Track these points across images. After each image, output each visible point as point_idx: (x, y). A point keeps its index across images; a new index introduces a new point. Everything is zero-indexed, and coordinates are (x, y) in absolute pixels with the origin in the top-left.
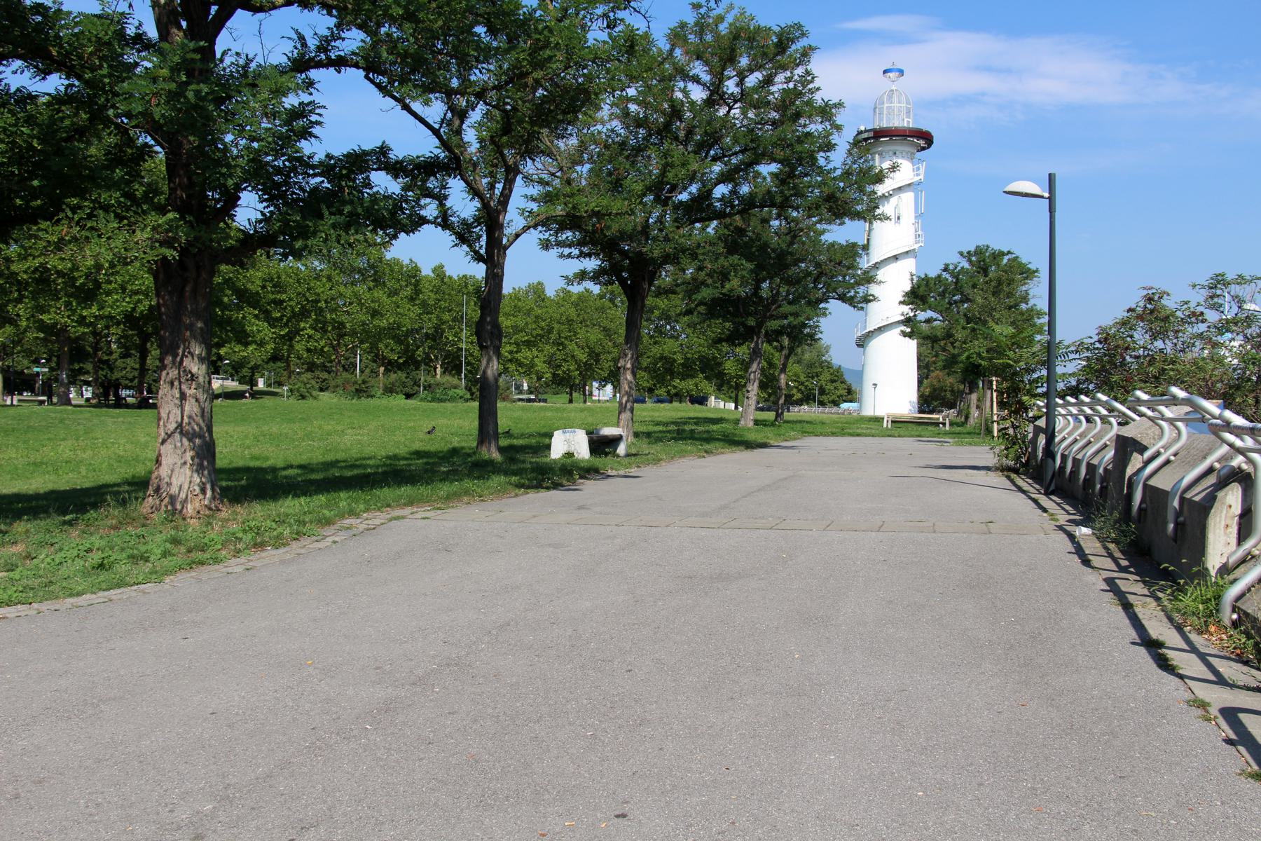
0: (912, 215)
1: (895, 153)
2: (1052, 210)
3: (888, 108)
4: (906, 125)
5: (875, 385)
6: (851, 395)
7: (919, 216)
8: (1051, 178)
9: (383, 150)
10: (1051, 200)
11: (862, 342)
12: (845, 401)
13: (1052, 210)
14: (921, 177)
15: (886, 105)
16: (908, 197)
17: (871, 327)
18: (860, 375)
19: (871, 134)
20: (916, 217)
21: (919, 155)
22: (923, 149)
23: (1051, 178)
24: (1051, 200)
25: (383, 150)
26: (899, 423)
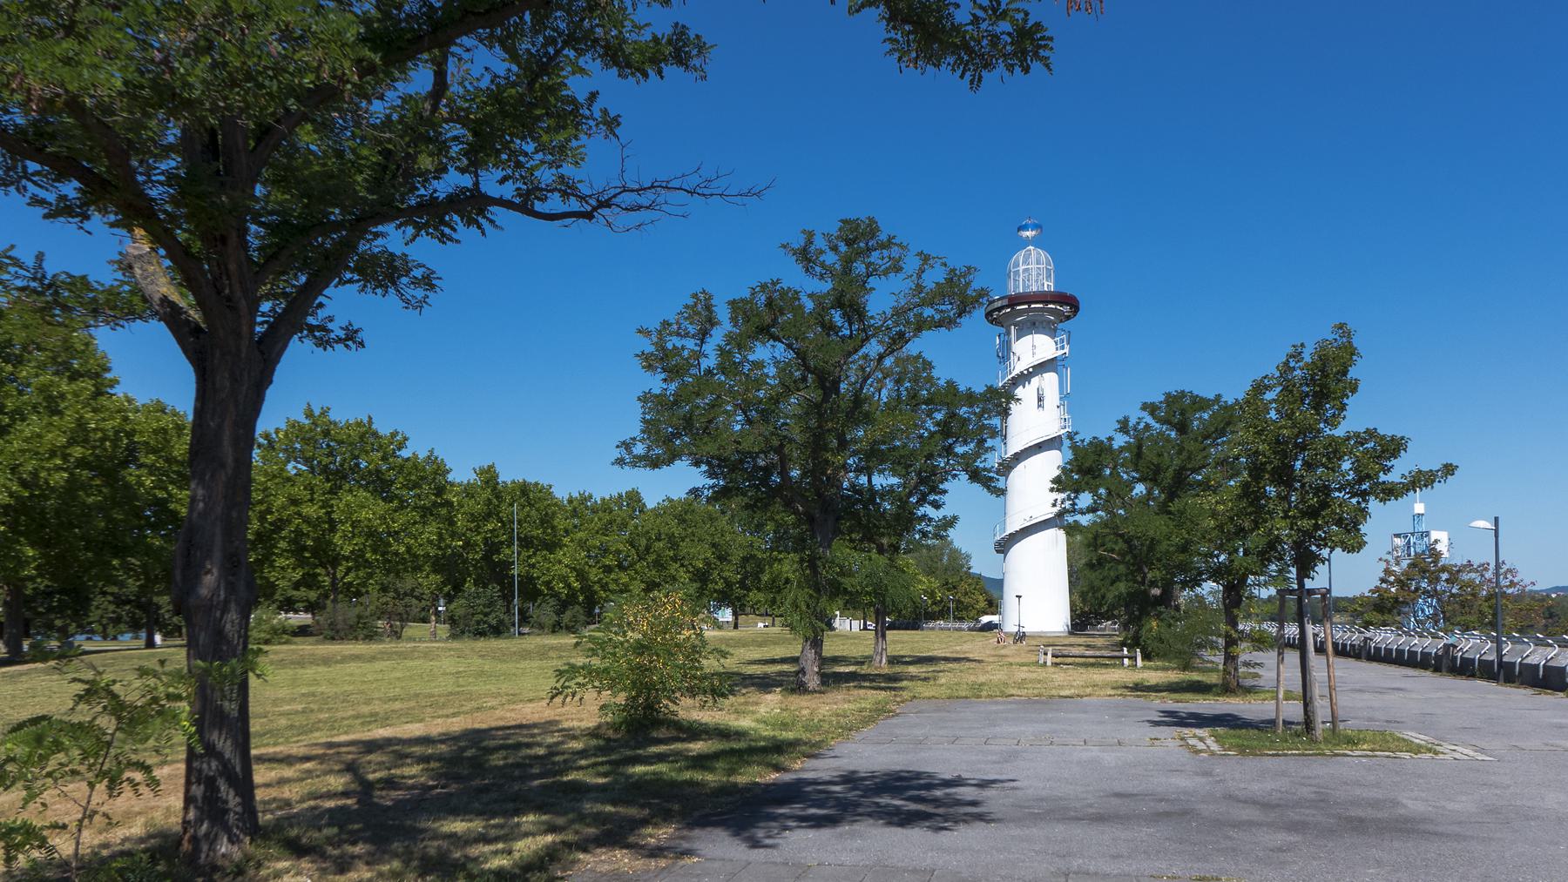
0: (1057, 396)
1: (1034, 324)
2: (1497, 536)
3: (1025, 270)
4: (1046, 289)
5: (1019, 597)
6: (993, 606)
7: (1064, 397)
8: (1496, 519)
9: (1470, 564)
10: (1496, 531)
11: (1004, 546)
12: (987, 614)
13: (1497, 536)
14: (1066, 350)
15: (1021, 268)
16: (1050, 381)
17: (1013, 526)
18: (999, 584)
19: (1005, 302)
20: (1061, 398)
21: (1066, 325)
22: (1068, 318)
23: (1496, 519)
24: (1496, 531)
25: (1470, 564)
26: (1048, 641)
